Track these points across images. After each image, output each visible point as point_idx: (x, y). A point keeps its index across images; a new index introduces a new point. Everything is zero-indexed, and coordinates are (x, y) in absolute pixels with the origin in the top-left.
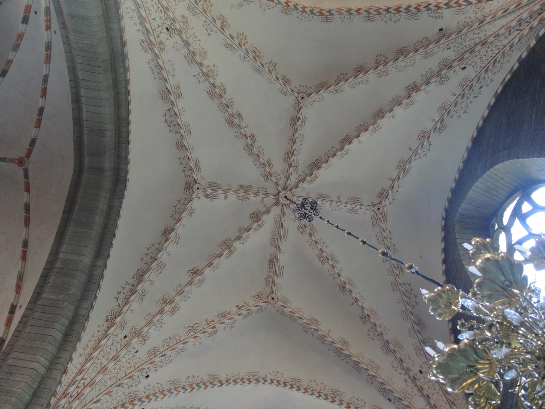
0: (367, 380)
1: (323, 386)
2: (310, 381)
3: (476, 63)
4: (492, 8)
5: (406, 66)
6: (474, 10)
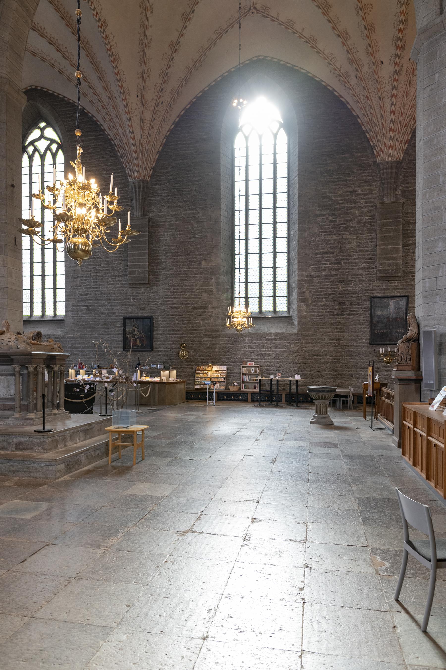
0: (138, 74)
1: (115, 45)
2: (112, 34)
4: (387, 103)
5: (361, 32)
6: (388, 90)
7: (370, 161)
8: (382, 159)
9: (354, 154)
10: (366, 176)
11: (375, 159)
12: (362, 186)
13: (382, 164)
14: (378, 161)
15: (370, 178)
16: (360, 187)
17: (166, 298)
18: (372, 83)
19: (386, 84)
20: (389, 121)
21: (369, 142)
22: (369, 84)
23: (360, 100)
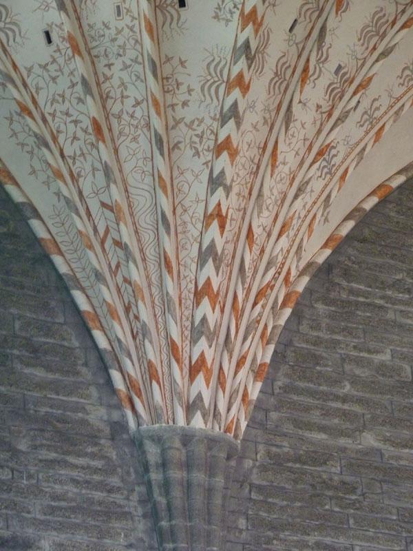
3: (54, 79)
6: (201, 121)
7: (91, 418)
8: (156, 414)
9: (18, 366)
10: (75, 481)
11: (116, 416)
12: (61, 528)
13: (158, 439)
14: (132, 424)
15: (98, 495)
16: (46, 525)
17: (257, 71)
18: (125, 76)
19: (190, 91)
20: (194, 252)
21: (89, 331)
22: (107, 79)
23: (55, 139)
